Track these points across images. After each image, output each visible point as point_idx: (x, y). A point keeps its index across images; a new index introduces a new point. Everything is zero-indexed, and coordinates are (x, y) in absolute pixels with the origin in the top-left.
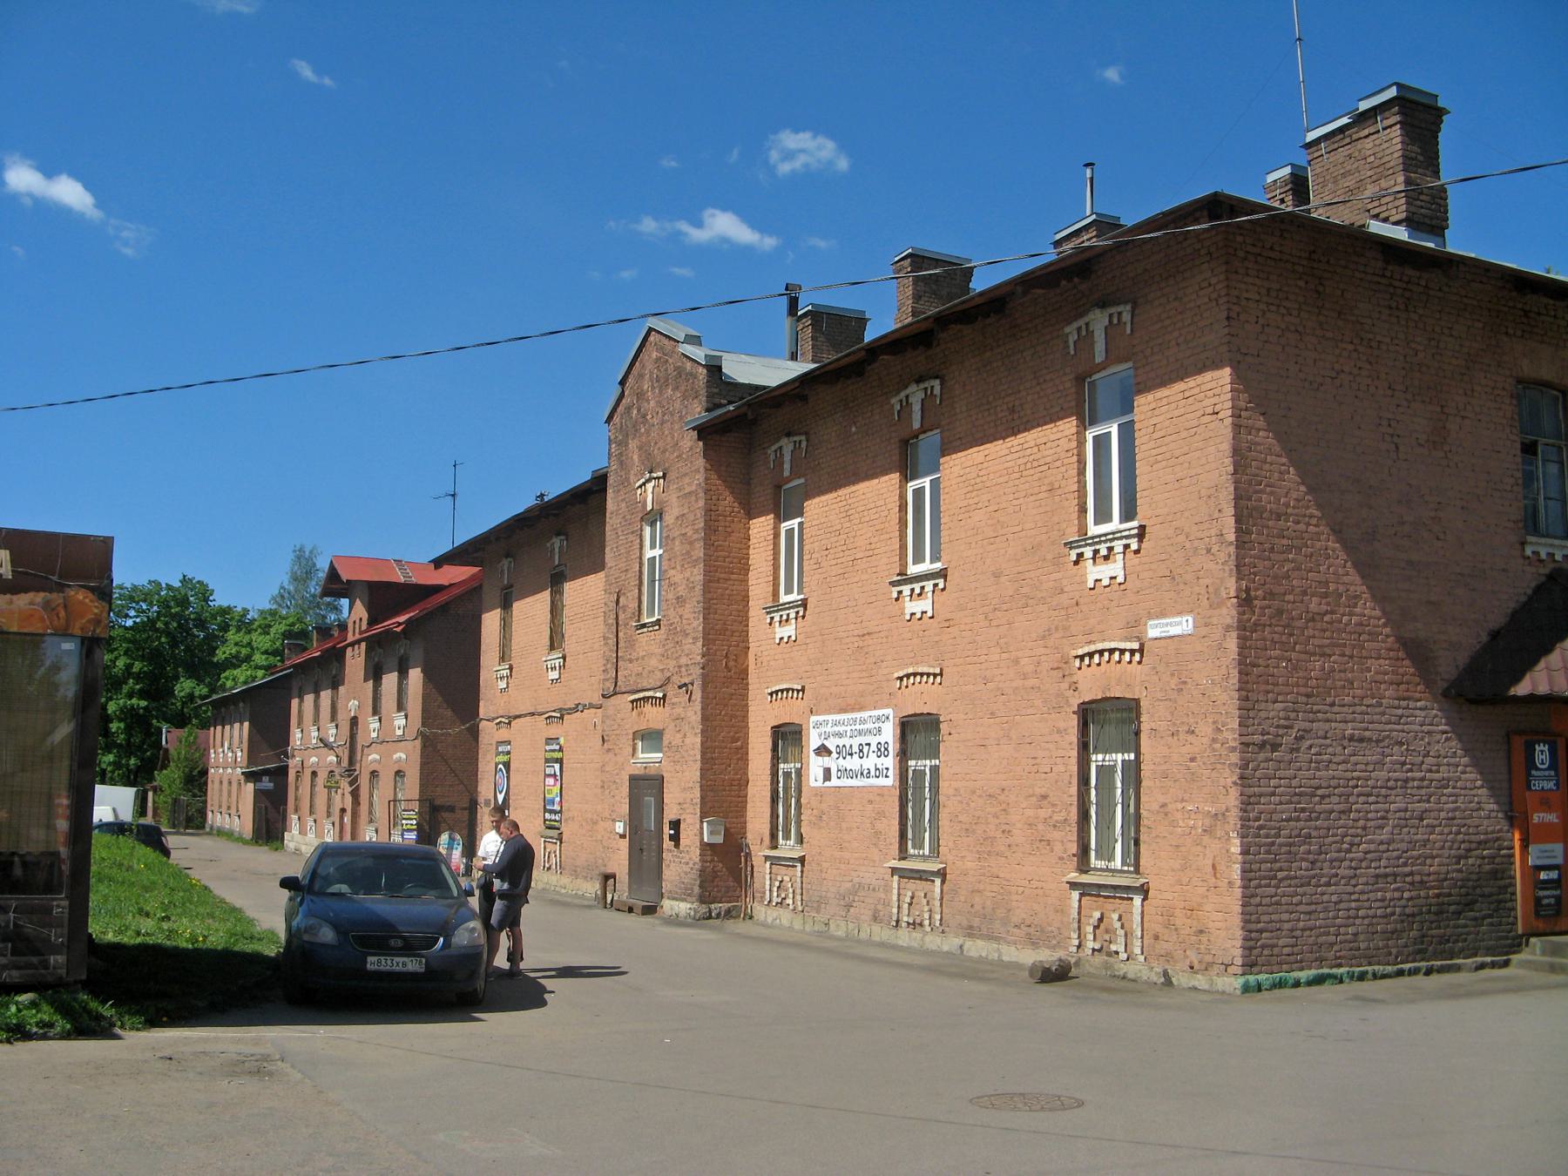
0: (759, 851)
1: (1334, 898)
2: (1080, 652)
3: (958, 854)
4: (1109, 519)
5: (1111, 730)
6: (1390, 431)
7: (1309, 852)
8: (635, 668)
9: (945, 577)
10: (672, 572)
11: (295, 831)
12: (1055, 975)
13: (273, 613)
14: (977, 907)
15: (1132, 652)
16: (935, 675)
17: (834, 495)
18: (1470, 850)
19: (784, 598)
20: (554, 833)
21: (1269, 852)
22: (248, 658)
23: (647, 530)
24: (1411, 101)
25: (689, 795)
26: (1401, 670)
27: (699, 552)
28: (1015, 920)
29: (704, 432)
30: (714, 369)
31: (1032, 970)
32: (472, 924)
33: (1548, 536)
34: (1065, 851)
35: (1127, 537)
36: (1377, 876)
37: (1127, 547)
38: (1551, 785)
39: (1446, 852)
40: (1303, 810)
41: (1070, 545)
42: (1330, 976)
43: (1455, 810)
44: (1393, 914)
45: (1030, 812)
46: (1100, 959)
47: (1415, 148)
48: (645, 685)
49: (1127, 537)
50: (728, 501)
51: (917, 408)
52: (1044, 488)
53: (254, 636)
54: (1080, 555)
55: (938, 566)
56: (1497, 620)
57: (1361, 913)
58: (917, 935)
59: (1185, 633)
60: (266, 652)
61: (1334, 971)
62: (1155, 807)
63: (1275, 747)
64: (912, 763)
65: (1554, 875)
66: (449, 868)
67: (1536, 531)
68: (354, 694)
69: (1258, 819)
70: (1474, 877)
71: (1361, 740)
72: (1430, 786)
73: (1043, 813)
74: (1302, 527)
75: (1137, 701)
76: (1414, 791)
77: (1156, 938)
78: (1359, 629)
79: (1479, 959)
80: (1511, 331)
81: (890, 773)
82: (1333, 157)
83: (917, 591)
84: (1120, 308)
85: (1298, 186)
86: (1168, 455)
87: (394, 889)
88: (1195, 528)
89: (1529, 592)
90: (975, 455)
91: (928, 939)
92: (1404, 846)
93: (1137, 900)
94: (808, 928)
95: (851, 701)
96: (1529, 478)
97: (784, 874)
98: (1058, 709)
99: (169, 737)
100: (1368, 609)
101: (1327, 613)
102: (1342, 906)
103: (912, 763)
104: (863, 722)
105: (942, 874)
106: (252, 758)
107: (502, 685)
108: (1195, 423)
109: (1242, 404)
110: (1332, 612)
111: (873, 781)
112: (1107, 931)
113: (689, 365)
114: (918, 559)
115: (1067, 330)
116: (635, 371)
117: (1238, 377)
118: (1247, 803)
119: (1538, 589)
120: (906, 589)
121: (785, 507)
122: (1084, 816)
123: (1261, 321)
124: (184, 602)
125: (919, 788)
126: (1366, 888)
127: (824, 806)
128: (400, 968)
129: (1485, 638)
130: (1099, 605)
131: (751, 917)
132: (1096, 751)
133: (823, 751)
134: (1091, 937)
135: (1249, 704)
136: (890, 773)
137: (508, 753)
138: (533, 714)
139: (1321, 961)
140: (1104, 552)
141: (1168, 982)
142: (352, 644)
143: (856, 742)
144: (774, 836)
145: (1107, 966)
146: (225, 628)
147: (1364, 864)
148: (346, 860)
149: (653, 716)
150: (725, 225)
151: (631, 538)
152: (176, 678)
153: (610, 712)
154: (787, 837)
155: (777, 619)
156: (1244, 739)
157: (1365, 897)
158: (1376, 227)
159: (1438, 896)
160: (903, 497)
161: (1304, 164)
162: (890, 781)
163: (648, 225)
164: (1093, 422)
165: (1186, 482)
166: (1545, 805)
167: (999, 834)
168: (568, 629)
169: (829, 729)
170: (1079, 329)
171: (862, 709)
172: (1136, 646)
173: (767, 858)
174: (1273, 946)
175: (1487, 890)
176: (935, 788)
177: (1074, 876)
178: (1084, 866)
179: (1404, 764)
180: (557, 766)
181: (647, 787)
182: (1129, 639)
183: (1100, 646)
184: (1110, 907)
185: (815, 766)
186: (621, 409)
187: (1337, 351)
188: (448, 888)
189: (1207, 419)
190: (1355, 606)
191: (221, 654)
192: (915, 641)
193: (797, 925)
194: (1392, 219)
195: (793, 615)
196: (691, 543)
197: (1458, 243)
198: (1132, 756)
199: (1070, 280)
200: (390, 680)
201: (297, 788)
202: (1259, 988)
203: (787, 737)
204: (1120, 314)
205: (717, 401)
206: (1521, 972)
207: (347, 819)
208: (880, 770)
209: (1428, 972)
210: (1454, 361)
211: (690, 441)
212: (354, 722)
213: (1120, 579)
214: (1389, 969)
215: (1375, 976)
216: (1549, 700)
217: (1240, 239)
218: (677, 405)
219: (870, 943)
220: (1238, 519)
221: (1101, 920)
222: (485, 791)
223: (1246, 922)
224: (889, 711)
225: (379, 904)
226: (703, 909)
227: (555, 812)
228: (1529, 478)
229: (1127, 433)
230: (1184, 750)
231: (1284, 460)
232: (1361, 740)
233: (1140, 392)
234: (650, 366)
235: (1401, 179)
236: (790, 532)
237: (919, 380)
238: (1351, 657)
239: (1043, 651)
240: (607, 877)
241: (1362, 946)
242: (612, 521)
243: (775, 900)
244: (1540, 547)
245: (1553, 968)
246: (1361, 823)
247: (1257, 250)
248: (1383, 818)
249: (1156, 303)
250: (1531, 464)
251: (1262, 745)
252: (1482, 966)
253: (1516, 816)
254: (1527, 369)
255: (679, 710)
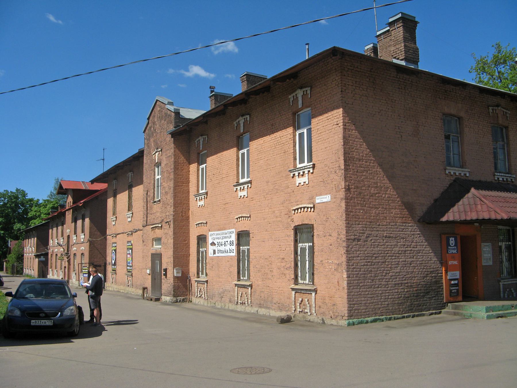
0: (194, 279)
1: (380, 292)
2: (294, 208)
3: (256, 278)
4: (304, 162)
5: (305, 236)
6: (399, 131)
7: (371, 277)
8: (153, 216)
9: (251, 183)
10: (164, 183)
11: (51, 275)
12: (286, 321)
13: (48, 201)
14: (262, 297)
15: (311, 208)
16: (248, 217)
17: (216, 156)
18: (428, 274)
19: (201, 192)
20: (130, 273)
21: (357, 277)
22: (39, 216)
23: (157, 169)
24: (407, 19)
25: (169, 260)
26: (403, 213)
27: (172, 176)
28: (274, 301)
29: (173, 135)
30: (177, 113)
31: (278, 319)
32: (71, 308)
33: (454, 167)
34: (290, 277)
35: (309, 168)
36: (395, 284)
37: (309, 171)
38: (455, 251)
39: (419, 275)
40: (369, 262)
41: (291, 171)
42: (379, 319)
43: (422, 261)
44: (401, 297)
45: (279, 264)
46: (302, 315)
47: (408, 35)
48: (156, 222)
49: (309, 168)
50: (182, 159)
51: (242, 125)
52: (282, 152)
53: (41, 208)
54: (294, 175)
55: (249, 179)
56: (437, 195)
57: (390, 297)
58: (243, 307)
59: (327, 201)
60: (45, 214)
61: (381, 317)
62: (319, 262)
63: (359, 240)
64: (241, 248)
65: (456, 282)
66: (68, 287)
67: (449, 164)
68: (68, 228)
69: (353, 265)
70: (429, 283)
71: (389, 237)
72: (416, 254)
73: (283, 264)
74: (368, 164)
75: (313, 225)
76: (408, 255)
77: (320, 307)
78: (388, 199)
79: (431, 311)
80: (441, 97)
81: (234, 251)
82: (386, 40)
83: (242, 188)
84: (306, 89)
85: (375, 49)
86: (322, 139)
87: (48, 295)
88: (331, 164)
89: (448, 186)
90: (261, 141)
91: (247, 308)
92: (405, 274)
93: (313, 294)
94: (209, 305)
95: (222, 227)
96: (448, 148)
97: (201, 286)
98: (287, 228)
99: (12, 244)
100: (391, 192)
101: (377, 193)
102: (383, 295)
103: (241, 248)
104: (226, 234)
105: (251, 286)
106: (38, 250)
107: (114, 223)
108: (331, 128)
109: (347, 121)
110: (379, 193)
111: (229, 254)
112: (304, 305)
113: (169, 112)
114: (243, 177)
115: (290, 97)
116: (152, 115)
117: (345, 112)
118: (349, 260)
119: (451, 185)
120: (239, 188)
121: (201, 161)
122: (296, 265)
123: (353, 92)
124: (17, 198)
125: (244, 256)
126: (392, 288)
127: (213, 263)
128: (44, 324)
129: (432, 202)
130: (300, 192)
131: (191, 302)
132: (300, 243)
133: (213, 244)
134: (299, 307)
135: (349, 225)
136: (234, 251)
137: (116, 246)
138: (123, 233)
139: (376, 314)
140: (301, 173)
141: (324, 322)
142: (68, 210)
143: (223, 241)
144: (198, 274)
145: (304, 317)
146: (31, 206)
147: (391, 280)
148: (30, 285)
149: (158, 233)
150: (197, 70)
151: (151, 172)
152: (15, 223)
153: (145, 231)
154: (202, 274)
155: (198, 199)
156: (347, 238)
157: (391, 291)
158: (395, 61)
159: (416, 290)
160: (238, 156)
161: (376, 43)
162: (234, 254)
163: (171, 71)
164: (299, 128)
165: (328, 148)
166: (453, 258)
167: (269, 272)
168: (134, 204)
169: (215, 236)
170: (293, 97)
171: (225, 229)
172: (312, 206)
173: (196, 281)
174: (359, 309)
175: (434, 288)
176: (248, 256)
177: (293, 286)
178: (296, 282)
179: (404, 245)
180: (131, 251)
181: (156, 257)
182: (309, 203)
183: (300, 206)
184: (305, 296)
185: (211, 249)
186: (148, 128)
187: (380, 103)
188: (68, 295)
189: (336, 126)
190: (387, 191)
191: (30, 215)
192: (242, 206)
193: (206, 304)
194: (400, 58)
195: (203, 198)
196: (170, 173)
197: (422, 66)
198: (311, 244)
199: (290, 79)
200: (79, 222)
201: (51, 260)
202: (354, 324)
203: (202, 239)
204: (307, 91)
205: (178, 124)
206: (445, 315)
207: (66, 270)
208: (231, 250)
209: (413, 317)
210: (421, 107)
211: (169, 138)
212: (69, 237)
213: (307, 183)
214: (400, 316)
215: (395, 319)
216: (453, 222)
217: (346, 64)
218: (165, 126)
219: (229, 310)
220: (345, 161)
221: (302, 301)
222: (109, 259)
223: (349, 301)
224: (234, 230)
225: (40, 302)
226: (175, 299)
227: (130, 266)
228: (448, 148)
229: (309, 131)
230: (328, 242)
231: (361, 140)
232: (389, 237)
233: (313, 118)
234: (157, 113)
235: (403, 45)
236: (203, 169)
237: (242, 116)
238: (386, 209)
239: (282, 208)
240: (144, 289)
241: (390, 308)
242: (146, 166)
243: (199, 295)
244: (451, 170)
245: (455, 314)
246: (390, 266)
247: (352, 68)
248: (397, 264)
249: (318, 87)
250: (448, 142)
251: (354, 240)
252: (432, 314)
253: (443, 262)
254: (446, 110)
255: (166, 231)
